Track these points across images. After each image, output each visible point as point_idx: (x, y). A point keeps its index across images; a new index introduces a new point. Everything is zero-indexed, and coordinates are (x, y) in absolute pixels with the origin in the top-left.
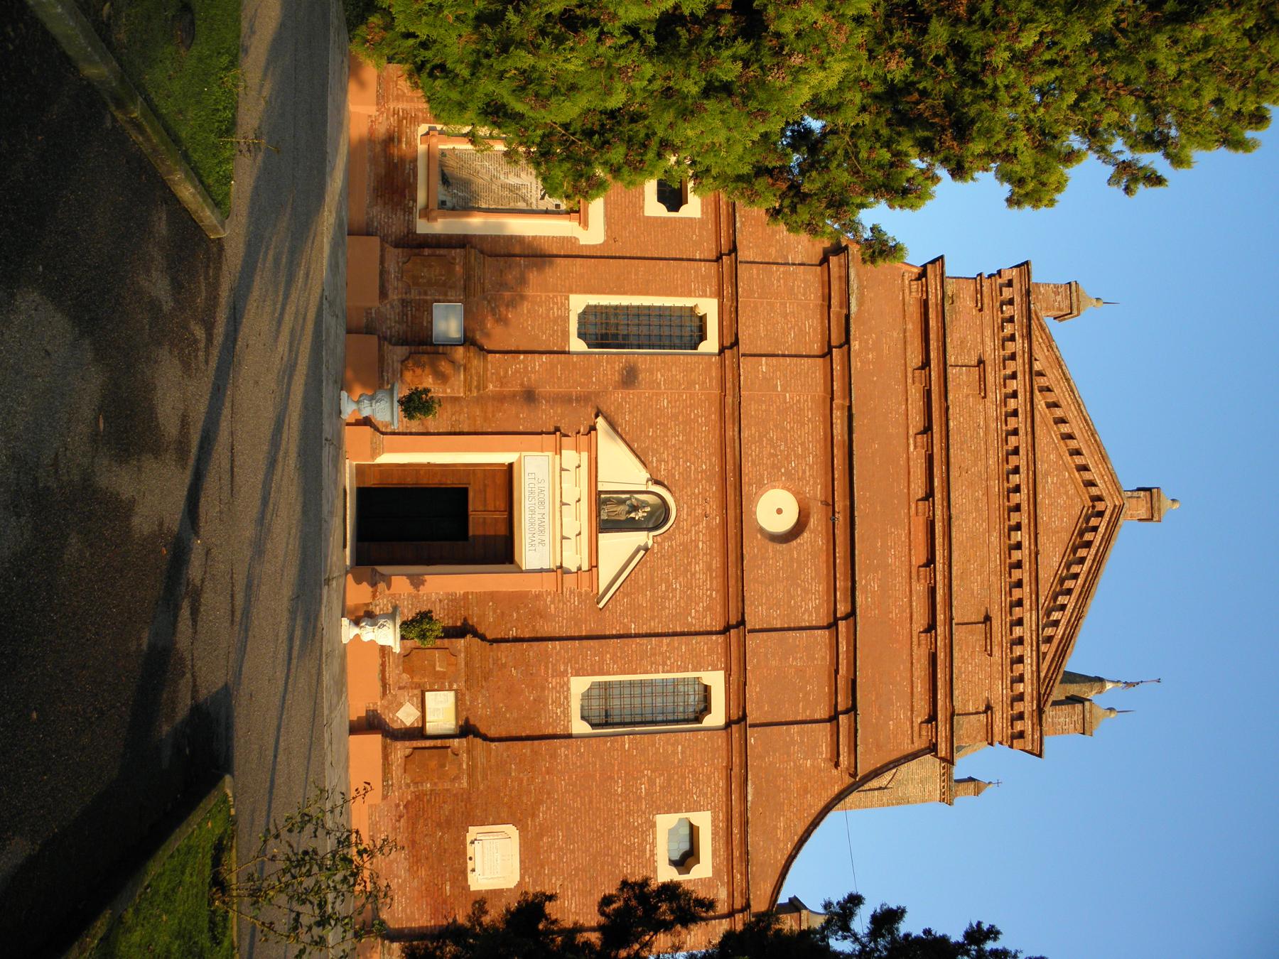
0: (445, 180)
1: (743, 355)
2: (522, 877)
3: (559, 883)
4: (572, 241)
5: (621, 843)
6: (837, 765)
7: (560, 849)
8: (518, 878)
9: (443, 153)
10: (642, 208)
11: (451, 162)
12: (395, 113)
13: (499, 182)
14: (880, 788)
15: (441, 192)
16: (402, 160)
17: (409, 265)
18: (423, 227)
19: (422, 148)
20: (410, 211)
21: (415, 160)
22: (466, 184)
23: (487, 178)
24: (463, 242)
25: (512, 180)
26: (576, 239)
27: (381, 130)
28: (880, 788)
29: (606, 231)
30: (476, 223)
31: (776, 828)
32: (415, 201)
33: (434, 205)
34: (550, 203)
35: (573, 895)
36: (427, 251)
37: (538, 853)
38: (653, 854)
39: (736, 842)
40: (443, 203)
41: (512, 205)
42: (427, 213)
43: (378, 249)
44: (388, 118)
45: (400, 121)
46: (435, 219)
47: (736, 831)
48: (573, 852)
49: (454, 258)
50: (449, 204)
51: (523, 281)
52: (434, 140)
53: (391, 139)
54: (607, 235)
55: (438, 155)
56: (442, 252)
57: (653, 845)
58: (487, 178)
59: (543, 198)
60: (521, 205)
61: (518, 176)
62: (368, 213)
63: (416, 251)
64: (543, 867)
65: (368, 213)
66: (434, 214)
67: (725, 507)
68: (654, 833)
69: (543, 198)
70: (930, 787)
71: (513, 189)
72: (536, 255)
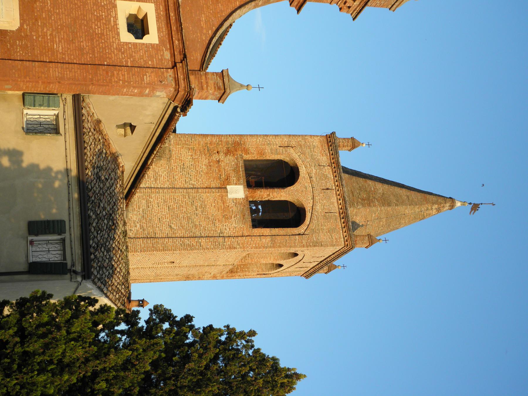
1: (190, 70)
2: (22, 25)
3: (49, 33)
5: (93, 14)
7: (49, 11)
8: (18, 25)
14: (299, 234)
28: (299, 234)
31: (200, 20)
34: (62, 105)
35: (60, 41)
37: (33, 11)
38: (116, 24)
39: (173, 21)
47: (172, 14)
48: (59, 14)
57: (116, 18)
64: (36, 20)
67: (175, 75)
68: (116, 12)
70: (335, 236)
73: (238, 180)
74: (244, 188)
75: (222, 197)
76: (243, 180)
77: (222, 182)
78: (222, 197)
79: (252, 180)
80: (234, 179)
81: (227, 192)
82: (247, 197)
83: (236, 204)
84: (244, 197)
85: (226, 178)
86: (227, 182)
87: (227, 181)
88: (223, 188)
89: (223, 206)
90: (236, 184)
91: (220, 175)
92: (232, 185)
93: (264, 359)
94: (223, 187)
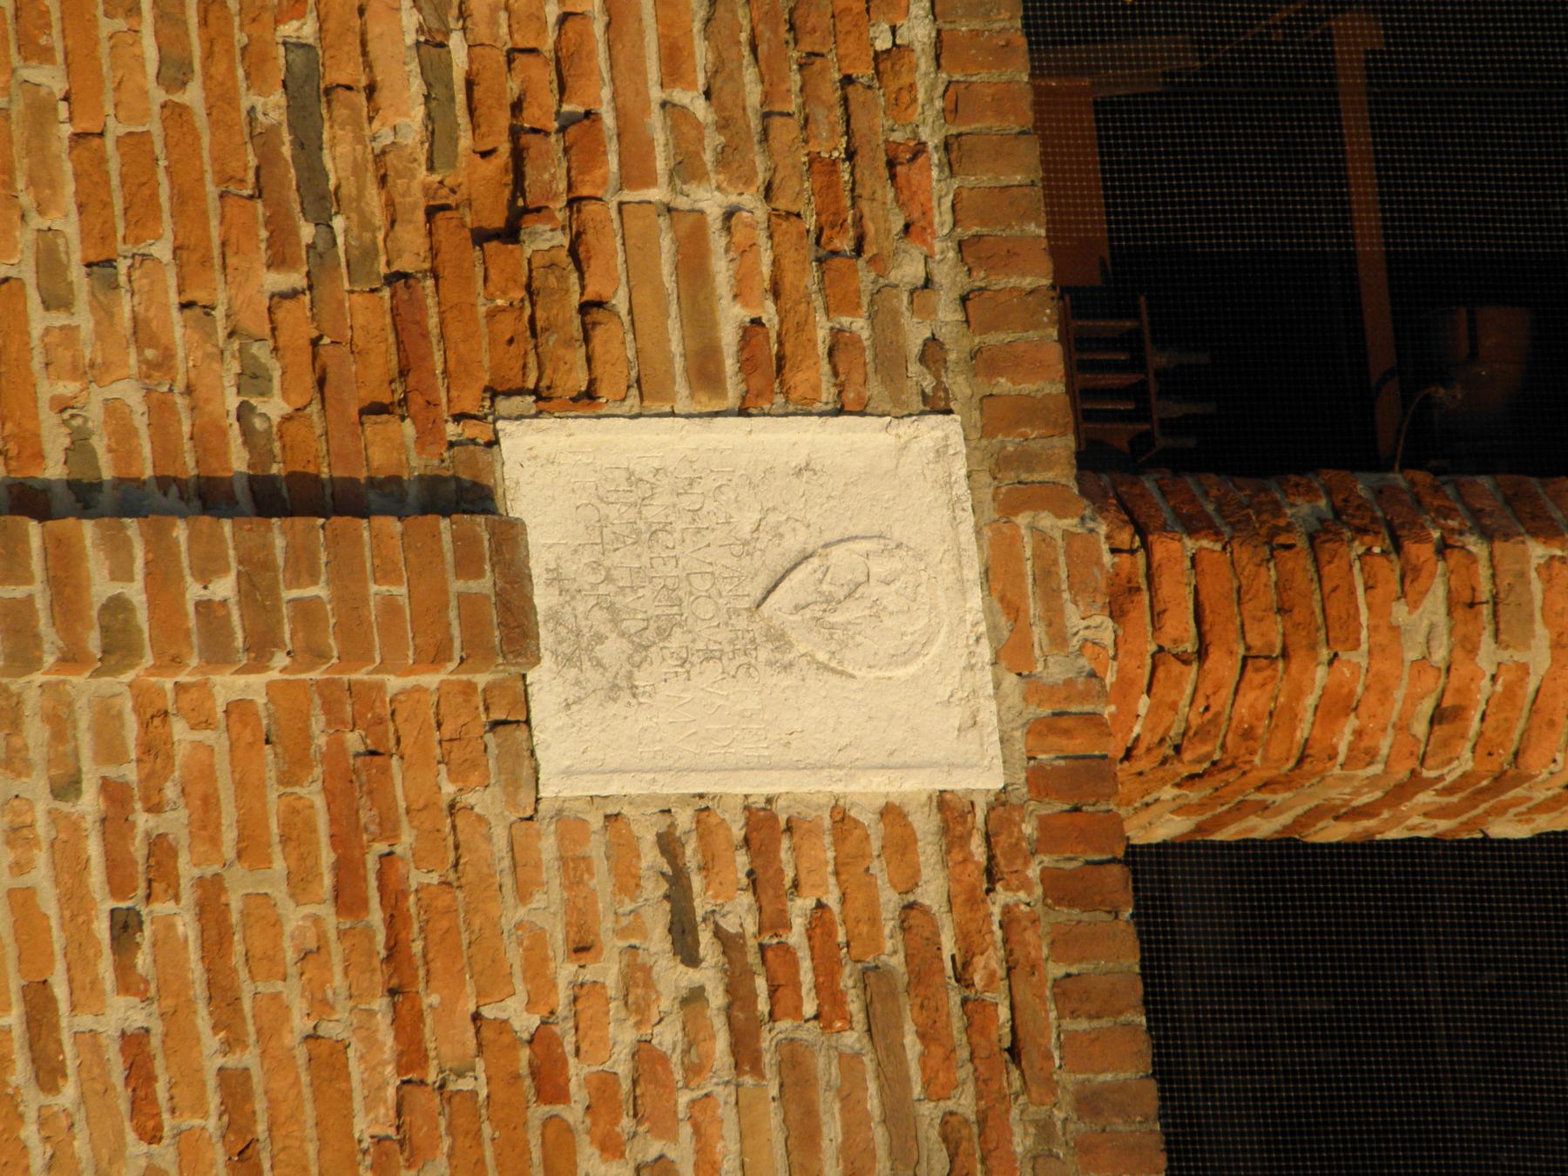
73: (838, 245)
74: (1005, 488)
75: (357, 781)
76: (965, 237)
77: (367, 314)
78: (357, 781)
79: (1120, 436)
80: (690, 209)
81: (514, 628)
82: (1070, 768)
83: (759, 972)
84: (983, 774)
85: (480, 183)
86: (488, 289)
87: (515, 275)
88: (380, 498)
89: (372, 1072)
90: (766, 378)
91: (309, 94)
92: (646, 394)
93: (17, 863)
94: (396, 449)
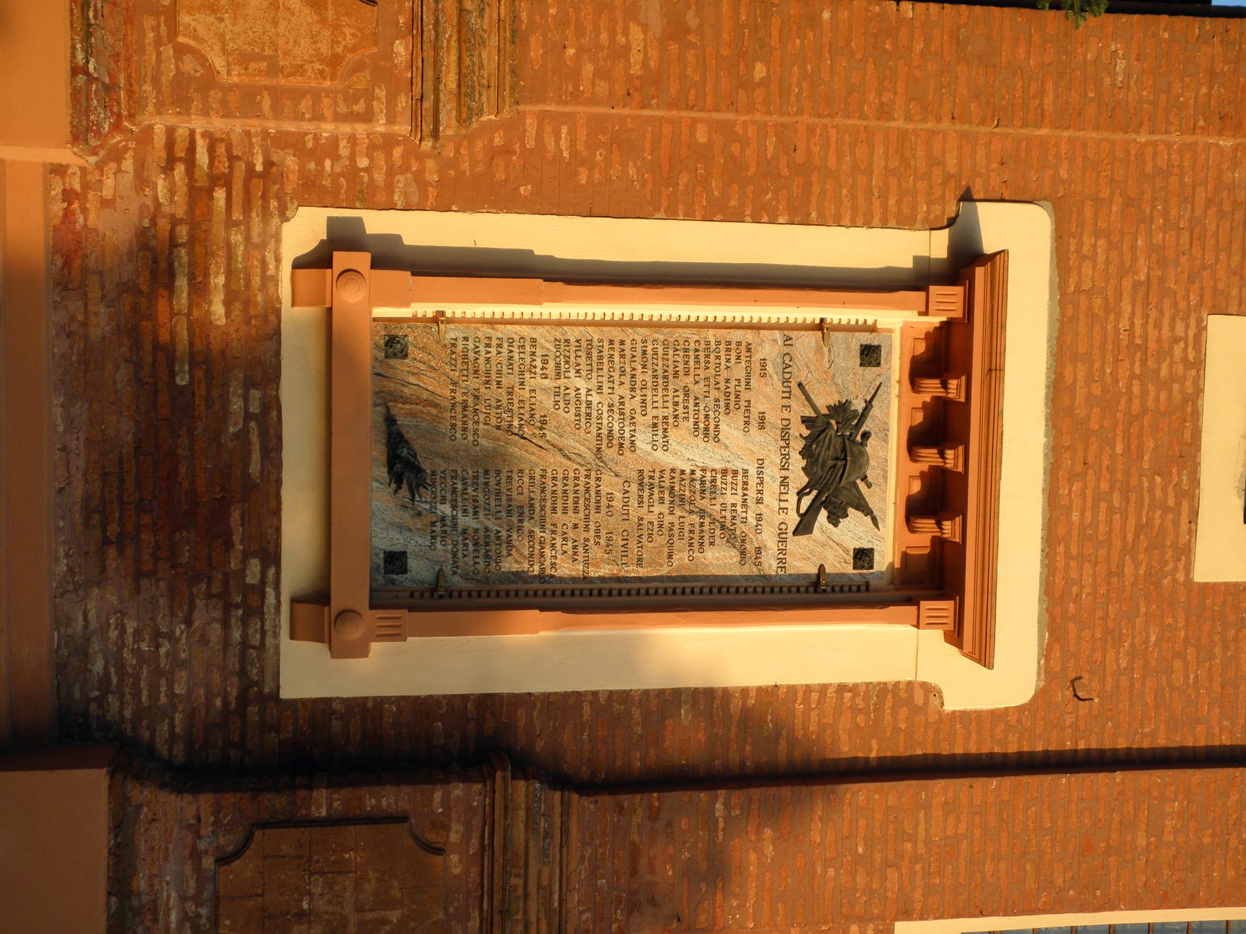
0: (404, 466)
4: (911, 698)
6: (800, 385)
9: (393, 345)
10: (1185, 552)
11: (424, 377)
12: (177, 154)
13: (629, 465)
15: (384, 519)
16: (211, 363)
17: (245, 868)
18: (308, 673)
19: (296, 318)
20: (251, 604)
21: (265, 374)
22: (487, 474)
23: (580, 444)
24: (478, 742)
25: (686, 453)
26: (930, 690)
27: (112, 220)
29: (1046, 653)
30: (528, 656)
32: (271, 556)
33: (351, 588)
36: (322, 802)
40: (395, 561)
41: (682, 562)
42: (319, 611)
43: (102, 822)
44: (142, 181)
45: (198, 195)
46: (360, 651)
49: (442, 825)
50: (419, 569)
51: (714, 872)
52: (350, 297)
53: (159, 260)
54: (1048, 672)
55: (366, 347)
56: (389, 798)
58: (580, 444)
59: (805, 526)
60: (719, 560)
61: (709, 433)
62: (61, 620)
63: (277, 802)
65: (61, 620)
66: (353, 633)
69: (805, 526)
71: (687, 491)
72: (775, 762)
